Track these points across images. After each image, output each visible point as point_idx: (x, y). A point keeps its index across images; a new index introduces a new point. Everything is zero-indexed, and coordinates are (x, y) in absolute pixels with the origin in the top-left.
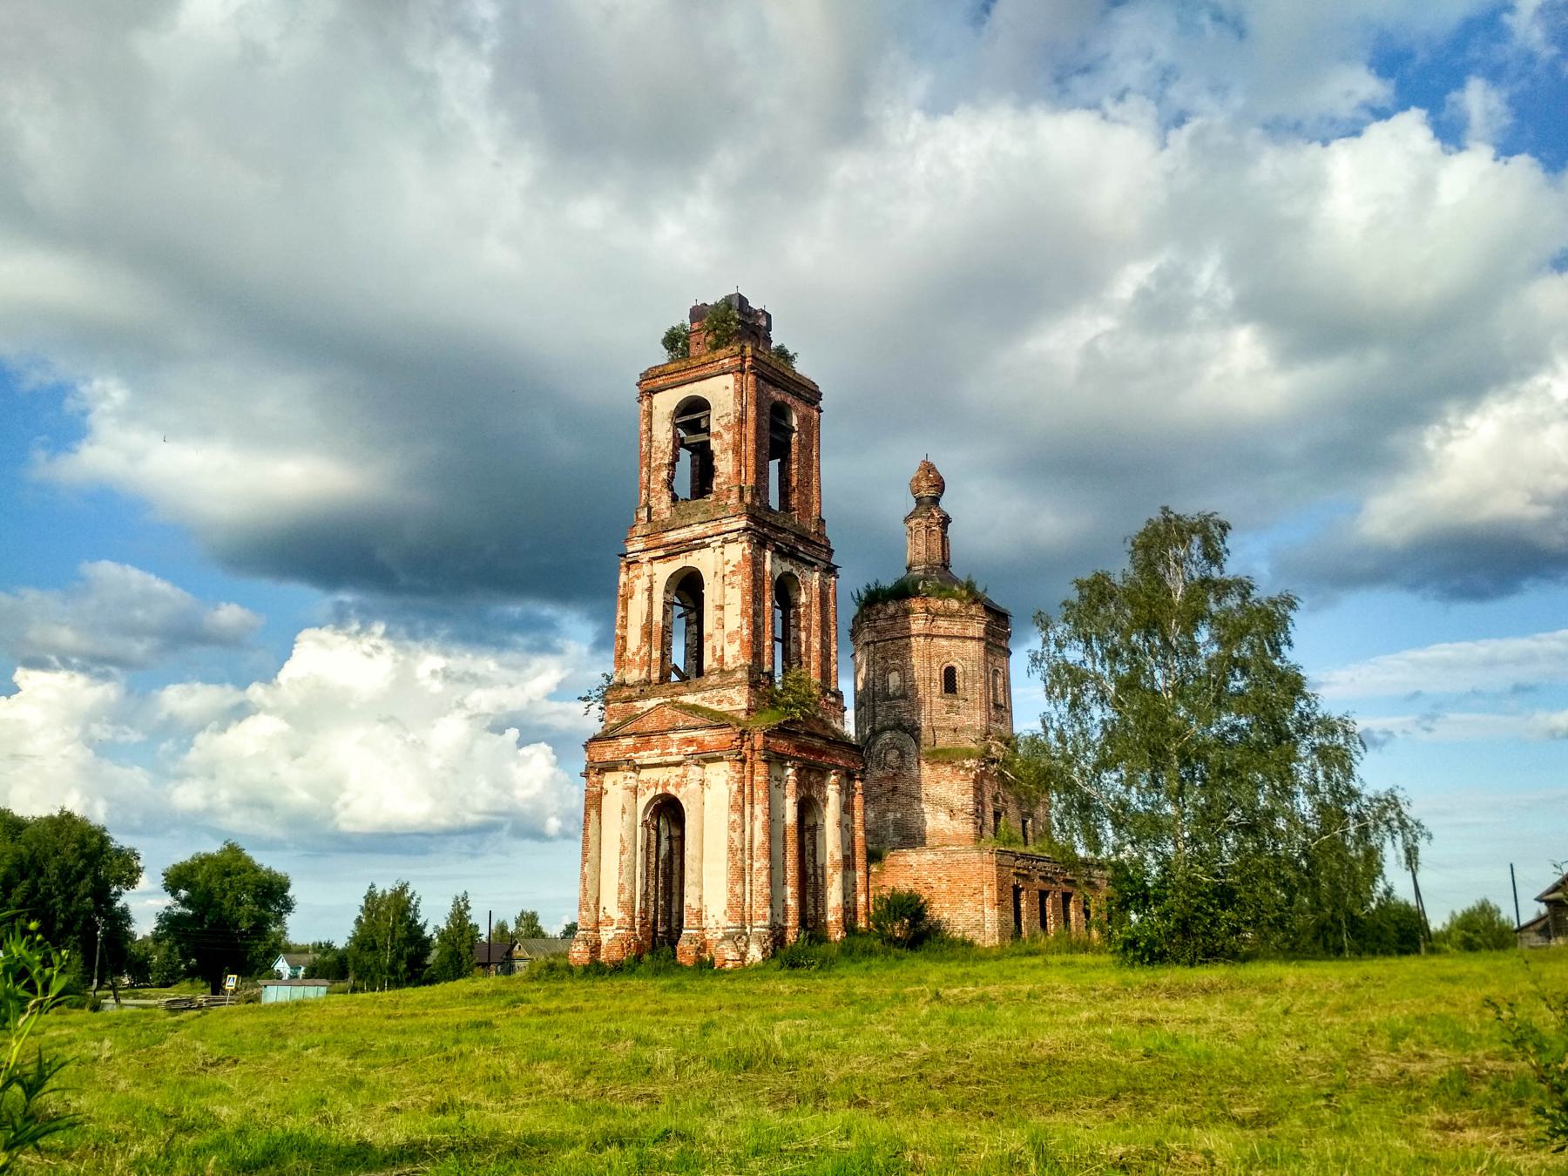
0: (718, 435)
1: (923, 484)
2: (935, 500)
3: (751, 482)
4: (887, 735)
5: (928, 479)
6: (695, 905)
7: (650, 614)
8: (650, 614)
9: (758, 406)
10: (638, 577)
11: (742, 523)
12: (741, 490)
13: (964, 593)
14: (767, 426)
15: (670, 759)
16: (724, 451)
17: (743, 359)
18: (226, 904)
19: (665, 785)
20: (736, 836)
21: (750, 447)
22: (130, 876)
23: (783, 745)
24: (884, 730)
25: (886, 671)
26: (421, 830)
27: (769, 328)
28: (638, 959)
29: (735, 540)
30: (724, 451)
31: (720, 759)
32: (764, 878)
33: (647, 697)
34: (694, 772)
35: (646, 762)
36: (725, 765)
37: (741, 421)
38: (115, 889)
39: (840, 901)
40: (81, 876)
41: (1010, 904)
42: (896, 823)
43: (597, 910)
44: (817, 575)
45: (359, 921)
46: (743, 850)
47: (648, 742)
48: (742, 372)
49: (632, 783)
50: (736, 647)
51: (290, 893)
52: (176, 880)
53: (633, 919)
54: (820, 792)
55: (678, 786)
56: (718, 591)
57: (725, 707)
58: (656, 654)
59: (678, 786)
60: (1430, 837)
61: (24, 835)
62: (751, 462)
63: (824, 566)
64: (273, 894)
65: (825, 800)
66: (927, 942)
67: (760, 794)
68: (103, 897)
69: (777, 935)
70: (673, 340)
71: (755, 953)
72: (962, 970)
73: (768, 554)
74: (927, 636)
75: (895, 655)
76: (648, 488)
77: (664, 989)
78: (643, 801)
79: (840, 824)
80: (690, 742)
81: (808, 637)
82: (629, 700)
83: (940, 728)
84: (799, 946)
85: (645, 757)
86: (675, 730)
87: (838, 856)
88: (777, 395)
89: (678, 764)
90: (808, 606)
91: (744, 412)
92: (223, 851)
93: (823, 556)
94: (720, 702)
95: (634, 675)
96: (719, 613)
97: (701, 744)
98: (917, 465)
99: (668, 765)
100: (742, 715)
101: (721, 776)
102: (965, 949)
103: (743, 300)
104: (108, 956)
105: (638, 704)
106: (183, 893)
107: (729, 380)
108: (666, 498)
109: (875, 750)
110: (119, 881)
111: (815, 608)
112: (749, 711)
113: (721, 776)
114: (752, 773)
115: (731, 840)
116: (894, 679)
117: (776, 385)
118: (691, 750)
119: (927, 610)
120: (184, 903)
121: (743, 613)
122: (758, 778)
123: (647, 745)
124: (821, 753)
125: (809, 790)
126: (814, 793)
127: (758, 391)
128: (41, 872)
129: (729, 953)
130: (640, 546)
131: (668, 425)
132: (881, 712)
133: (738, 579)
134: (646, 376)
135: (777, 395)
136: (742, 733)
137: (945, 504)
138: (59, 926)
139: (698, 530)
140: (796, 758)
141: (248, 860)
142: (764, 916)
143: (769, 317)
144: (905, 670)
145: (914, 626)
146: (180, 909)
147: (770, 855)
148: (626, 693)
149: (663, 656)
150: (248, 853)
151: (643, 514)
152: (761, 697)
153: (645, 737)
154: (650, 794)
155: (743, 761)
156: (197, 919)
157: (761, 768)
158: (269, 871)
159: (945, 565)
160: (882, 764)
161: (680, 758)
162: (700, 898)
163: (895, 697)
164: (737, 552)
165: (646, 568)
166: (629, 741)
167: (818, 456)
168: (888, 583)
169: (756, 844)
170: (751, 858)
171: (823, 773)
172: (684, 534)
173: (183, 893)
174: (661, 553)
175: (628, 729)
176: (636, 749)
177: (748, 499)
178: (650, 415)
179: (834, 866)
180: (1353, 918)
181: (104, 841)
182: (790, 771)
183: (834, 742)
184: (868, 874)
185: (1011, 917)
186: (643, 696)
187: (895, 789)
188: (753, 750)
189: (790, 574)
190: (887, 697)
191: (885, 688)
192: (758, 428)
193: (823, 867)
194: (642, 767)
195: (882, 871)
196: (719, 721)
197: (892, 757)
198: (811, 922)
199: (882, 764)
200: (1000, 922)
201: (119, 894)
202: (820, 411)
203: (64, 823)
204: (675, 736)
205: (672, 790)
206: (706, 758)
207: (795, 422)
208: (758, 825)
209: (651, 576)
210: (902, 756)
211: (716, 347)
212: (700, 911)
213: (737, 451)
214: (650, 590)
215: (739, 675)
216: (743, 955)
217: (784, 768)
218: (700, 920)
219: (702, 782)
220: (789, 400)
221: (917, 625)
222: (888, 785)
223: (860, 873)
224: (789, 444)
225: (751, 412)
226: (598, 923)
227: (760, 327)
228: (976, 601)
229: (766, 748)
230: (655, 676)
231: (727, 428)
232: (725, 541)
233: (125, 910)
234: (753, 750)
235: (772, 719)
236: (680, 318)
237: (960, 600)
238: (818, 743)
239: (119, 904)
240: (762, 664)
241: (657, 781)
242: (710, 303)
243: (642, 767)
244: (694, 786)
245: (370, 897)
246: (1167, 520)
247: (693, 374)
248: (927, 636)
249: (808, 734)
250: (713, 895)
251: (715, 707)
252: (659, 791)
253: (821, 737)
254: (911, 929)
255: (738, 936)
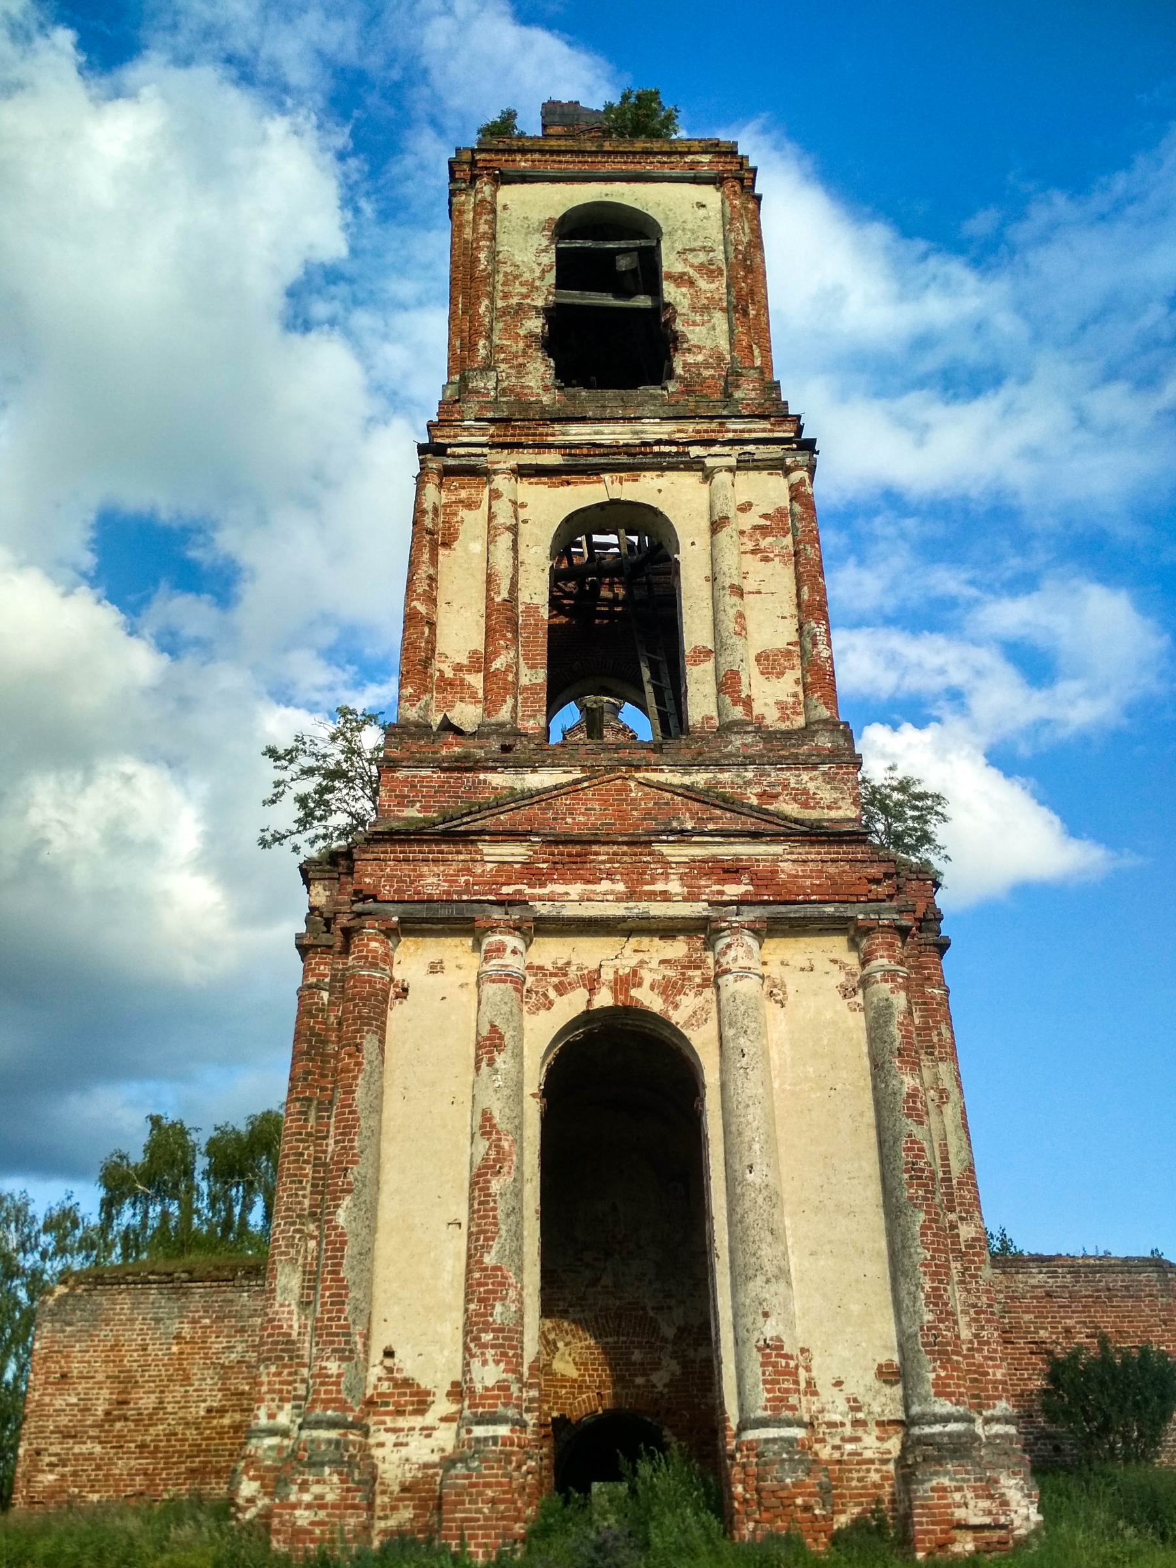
19: (624, 983)
26: (424, 936)
35: (571, 910)
47: (580, 860)
55: (669, 989)
59: (669, 989)
80: (732, 871)
82: (465, 765)
85: (572, 897)
97: (764, 879)
105: (497, 779)
118: (733, 890)
148: (454, 748)
161: (698, 909)
166: (514, 852)
176: (530, 873)
180: (167, 1551)
205: (649, 999)
242: (565, 101)
252: (604, 999)
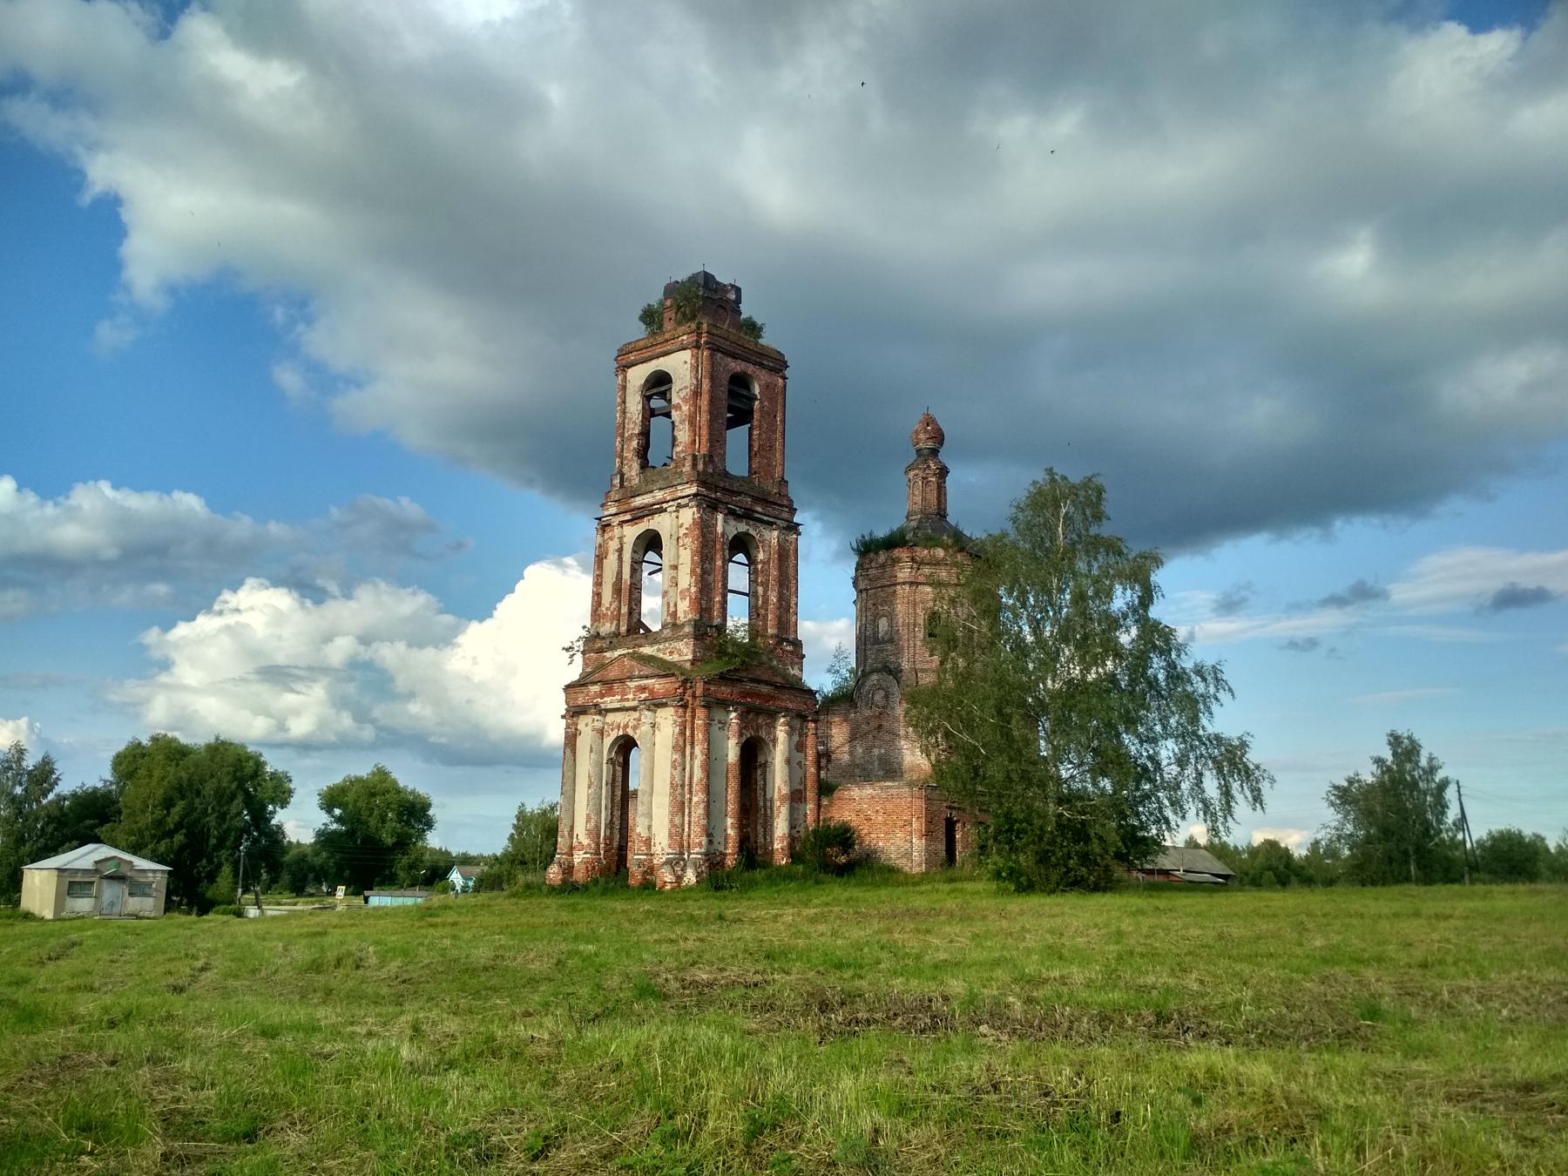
0: (678, 407)
1: (922, 436)
2: (934, 452)
3: (704, 450)
4: (875, 677)
5: (926, 431)
6: (645, 834)
7: (620, 573)
8: (620, 573)
9: (713, 379)
10: (611, 539)
11: (694, 490)
12: (695, 458)
13: (950, 542)
14: (724, 396)
15: (627, 704)
16: (682, 422)
17: (699, 335)
18: (373, 822)
19: (626, 726)
20: (677, 773)
21: (704, 418)
22: (282, 795)
23: (724, 691)
24: (872, 672)
25: (877, 617)
27: (738, 301)
28: (595, 882)
29: (686, 506)
30: (682, 422)
31: (664, 705)
32: (701, 811)
33: (615, 649)
34: (647, 716)
36: (670, 711)
37: (696, 394)
38: (270, 807)
39: (786, 831)
40: (233, 797)
41: (941, 834)
42: (880, 758)
43: (571, 837)
44: (776, 533)
45: (512, 837)
46: (683, 786)
48: (698, 347)
49: (598, 725)
50: (687, 602)
51: (431, 812)
52: (330, 800)
53: (598, 845)
54: (769, 733)
55: (635, 728)
56: (673, 552)
57: (675, 658)
58: (624, 610)
60: (1273, 781)
61: (187, 761)
62: (704, 432)
63: (785, 524)
64: (416, 813)
65: (775, 741)
66: (857, 871)
67: (699, 736)
68: (260, 817)
69: (713, 861)
70: (650, 317)
71: (690, 877)
72: (847, 894)
73: (720, 517)
74: (911, 583)
75: (884, 602)
76: (621, 457)
77: (560, 906)
78: (608, 741)
79: (788, 761)
80: (643, 689)
81: (765, 591)
82: (601, 651)
83: (923, 670)
84: (740, 868)
86: (631, 678)
87: (785, 790)
88: (736, 366)
89: (634, 709)
90: (766, 563)
91: (699, 385)
92: (374, 774)
93: (785, 515)
94: (671, 653)
95: (607, 628)
96: (673, 573)
97: (652, 692)
98: (920, 417)
99: (628, 709)
100: (688, 665)
101: (667, 719)
102: (888, 875)
103: (708, 277)
104: (273, 866)
105: (608, 654)
106: (337, 812)
107: (686, 355)
108: (636, 466)
109: (864, 691)
110: (273, 801)
111: (773, 565)
112: (693, 662)
113: (667, 719)
114: (693, 717)
115: (673, 777)
116: (883, 624)
117: (735, 357)
119: (913, 560)
120: (339, 820)
121: (693, 571)
122: (698, 722)
123: (610, 692)
124: (769, 698)
125: (757, 731)
126: (763, 734)
127: (713, 364)
128: (198, 793)
129: (667, 876)
130: (613, 510)
131: (638, 398)
132: (871, 655)
133: (688, 541)
134: (623, 352)
135: (736, 366)
136: (684, 682)
137: (943, 456)
138: (213, 841)
139: (659, 495)
140: (739, 703)
141: (395, 782)
142: (700, 845)
143: (738, 290)
144: (891, 616)
145: (900, 575)
146: (335, 826)
147: (708, 790)
149: (630, 613)
150: (393, 775)
151: (617, 481)
152: (708, 649)
153: (608, 685)
154: (614, 735)
155: (685, 706)
156: (351, 834)
157: (701, 713)
158: (413, 792)
159: (942, 514)
160: (871, 704)
162: (650, 827)
163: (884, 642)
164: (689, 515)
165: (617, 531)
166: (595, 688)
167: (783, 421)
168: (881, 533)
169: (695, 780)
170: (691, 792)
171: (773, 716)
172: (646, 499)
173: (337, 812)
174: (628, 517)
175: (597, 677)
177: (700, 467)
178: (624, 388)
179: (782, 799)
181: (259, 765)
182: (733, 715)
183: (782, 687)
184: (819, 806)
185: (942, 847)
186: (612, 648)
187: (880, 726)
188: (694, 697)
189: (747, 534)
190: (877, 641)
191: (876, 632)
192: (712, 401)
193: (772, 800)
194: (608, 711)
195: (831, 804)
196: (666, 670)
197: (879, 697)
198: (752, 852)
199: (871, 704)
200: (927, 851)
201: (274, 812)
202: (785, 378)
203: (220, 750)
204: (632, 684)
205: (630, 732)
206: (655, 704)
207: (757, 391)
208: (697, 763)
209: (621, 538)
210: (886, 697)
211: (679, 324)
212: (649, 839)
213: (692, 422)
214: (620, 551)
215: (687, 629)
216: (679, 878)
217: (729, 712)
218: (649, 847)
219: (653, 725)
220: (750, 369)
221: (904, 573)
222: (874, 724)
223: (810, 807)
224: (751, 411)
225: (706, 385)
226: (572, 848)
227: (728, 301)
228: (962, 550)
229: (706, 694)
230: (623, 629)
231: (684, 400)
232: (679, 506)
233: (279, 827)
234: (694, 697)
235: (715, 668)
236: (655, 297)
237: (946, 548)
238: (764, 689)
239: (273, 822)
240: (711, 618)
241: (619, 722)
243: (608, 711)
244: (645, 728)
245: (521, 816)
246: (1053, 480)
247: (659, 350)
248: (911, 583)
249: (752, 680)
250: (656, 827)
251: (668, 658)
253: (768, 683)
254: (835, 856)
255: (677, 862)
